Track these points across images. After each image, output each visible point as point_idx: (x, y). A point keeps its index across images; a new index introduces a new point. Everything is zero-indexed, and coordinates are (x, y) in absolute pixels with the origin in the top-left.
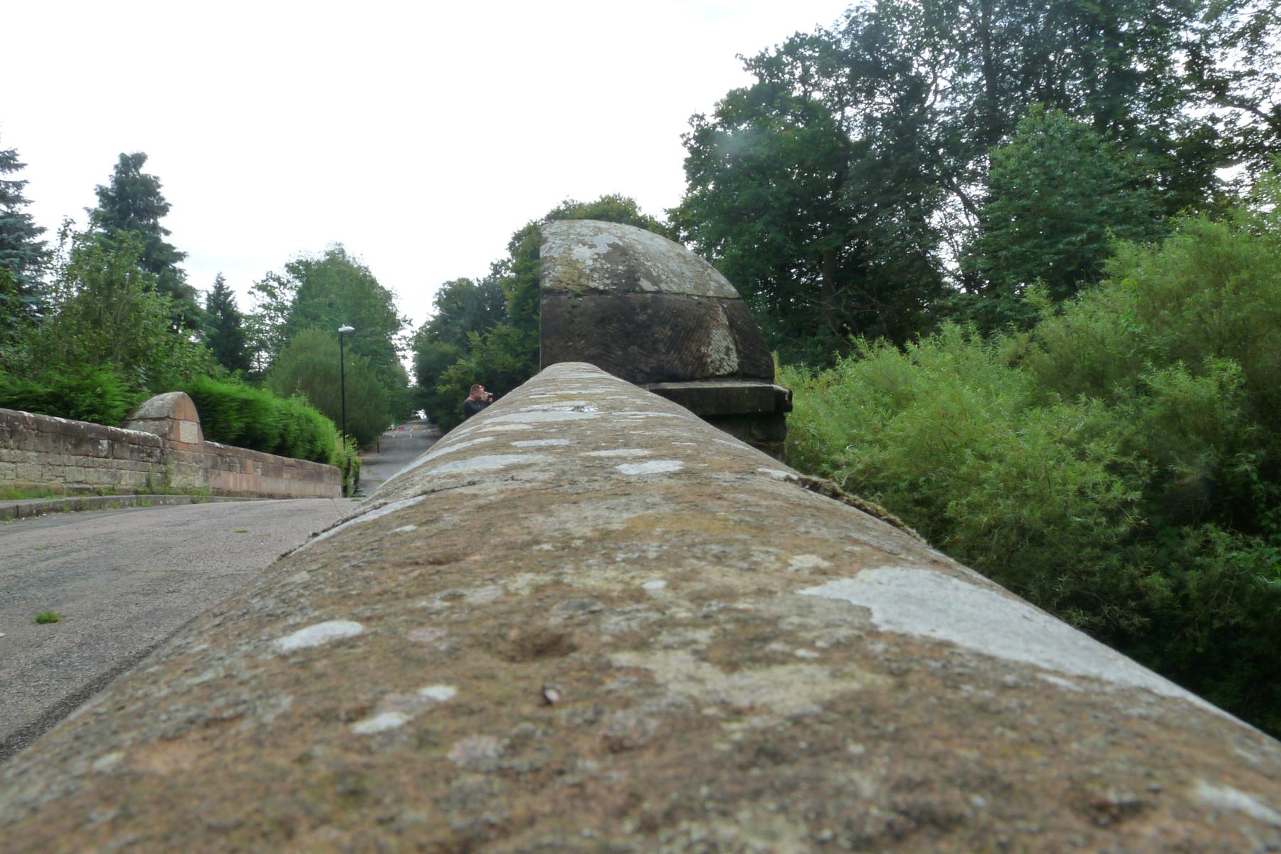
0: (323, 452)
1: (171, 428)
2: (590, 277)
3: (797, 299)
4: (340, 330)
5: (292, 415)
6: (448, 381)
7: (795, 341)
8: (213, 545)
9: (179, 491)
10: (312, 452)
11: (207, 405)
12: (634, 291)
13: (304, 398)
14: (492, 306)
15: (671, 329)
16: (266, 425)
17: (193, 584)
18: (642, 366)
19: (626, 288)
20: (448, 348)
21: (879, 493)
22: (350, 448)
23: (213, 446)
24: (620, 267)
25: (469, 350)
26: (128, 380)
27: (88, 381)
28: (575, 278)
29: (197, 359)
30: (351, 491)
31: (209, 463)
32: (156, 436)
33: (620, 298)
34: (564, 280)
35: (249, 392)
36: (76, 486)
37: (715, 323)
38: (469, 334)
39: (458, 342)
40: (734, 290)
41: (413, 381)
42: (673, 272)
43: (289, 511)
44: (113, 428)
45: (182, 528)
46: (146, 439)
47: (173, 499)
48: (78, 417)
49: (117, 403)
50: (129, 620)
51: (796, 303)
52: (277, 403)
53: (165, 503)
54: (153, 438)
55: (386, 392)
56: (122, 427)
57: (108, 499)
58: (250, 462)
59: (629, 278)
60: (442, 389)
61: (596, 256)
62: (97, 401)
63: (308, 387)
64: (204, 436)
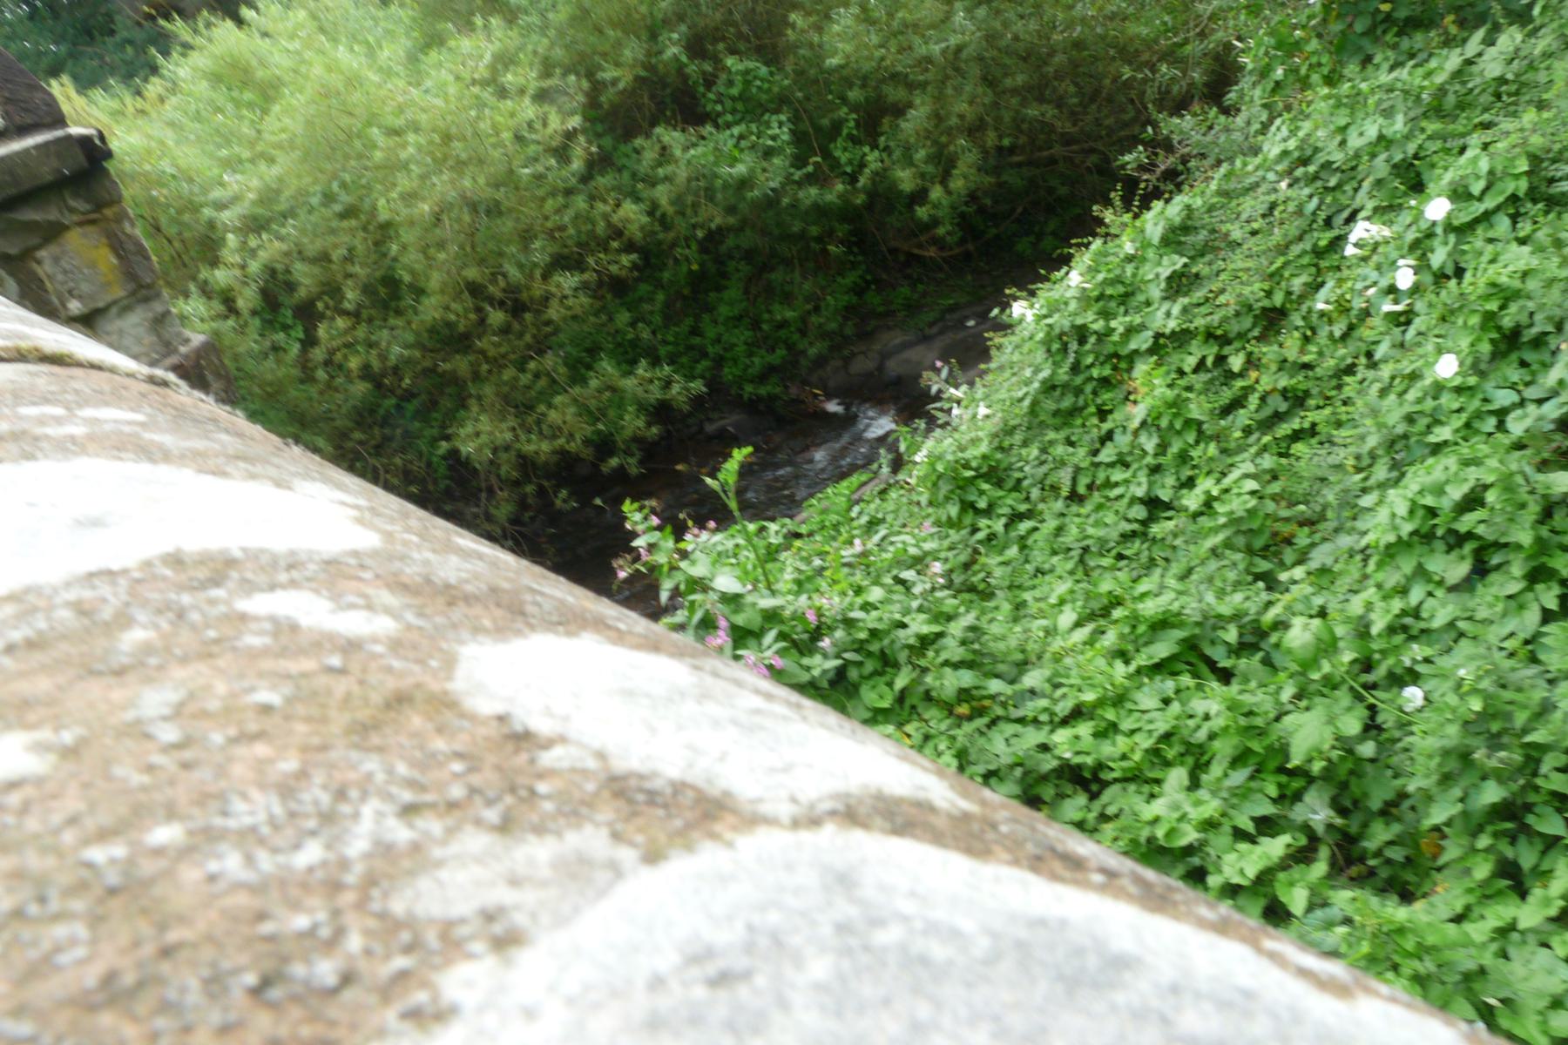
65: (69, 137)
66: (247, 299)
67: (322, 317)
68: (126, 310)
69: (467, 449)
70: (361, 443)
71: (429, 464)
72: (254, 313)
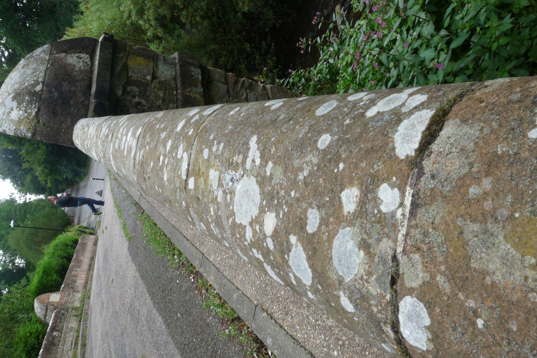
0: (73, 241)
1: (52, 305)
2: (30, 114)
3: (34, 8)
4: (12, 226)
5: (53, 253)
6: (46, 181)
7: (57, 15)
8: (117, 294)
9: (82, 303)
10: (72, 246)
11: (43, 289)
12: (41, 95)
13: (45, 247)
14: (10, 154)
15: (64, 82)
16: (56, 264)
17: (137, 304)
18: (81, 100)
19: (39, 99)
20: (28, 178)
21: (146, 2)
22: (71, 229)
23: (63, 288)
24: (27, 98)
25: (32, 169)
26: (25, 322)
27: (23, 339)
28: (29, 121)
29: (19, 291)
30: (92, 231)
31: (71, 290)
32: (55, 311)
33: (43, 103)
34: (29, 126)
35: (39, 270)
36: (73, 346)
37: (63, 60)
38: (23, 168)
39: (27, 173)
40: (46, 46)
41: (42, 197)
42: (32, 73)
43: (104, 260)
44: (48, 330)
45: (105, 305)
46: (55, 316)
47: (86, 306)
48: (40, 344)
49: (36, 327)
50: (150, 331)
51: (37, 9)
52: (46, 259)
53: (87, 310)
54: (55, 313)
55: (46, 210)
56: (48, 326)
57: (82, 333)
58: (73, 273)
59: (33, 95)
60: (49, 185)
61: (18, 109)
62: (33, 336)
63: (39, 244)
64: (57, 291)
65: (101, 42)
66: (160, 32)
67: (179, 16)
68: (157, 66)
69: (246, 9)
70: (220, 36)
71: (240, 23)
72: (164, 33)
